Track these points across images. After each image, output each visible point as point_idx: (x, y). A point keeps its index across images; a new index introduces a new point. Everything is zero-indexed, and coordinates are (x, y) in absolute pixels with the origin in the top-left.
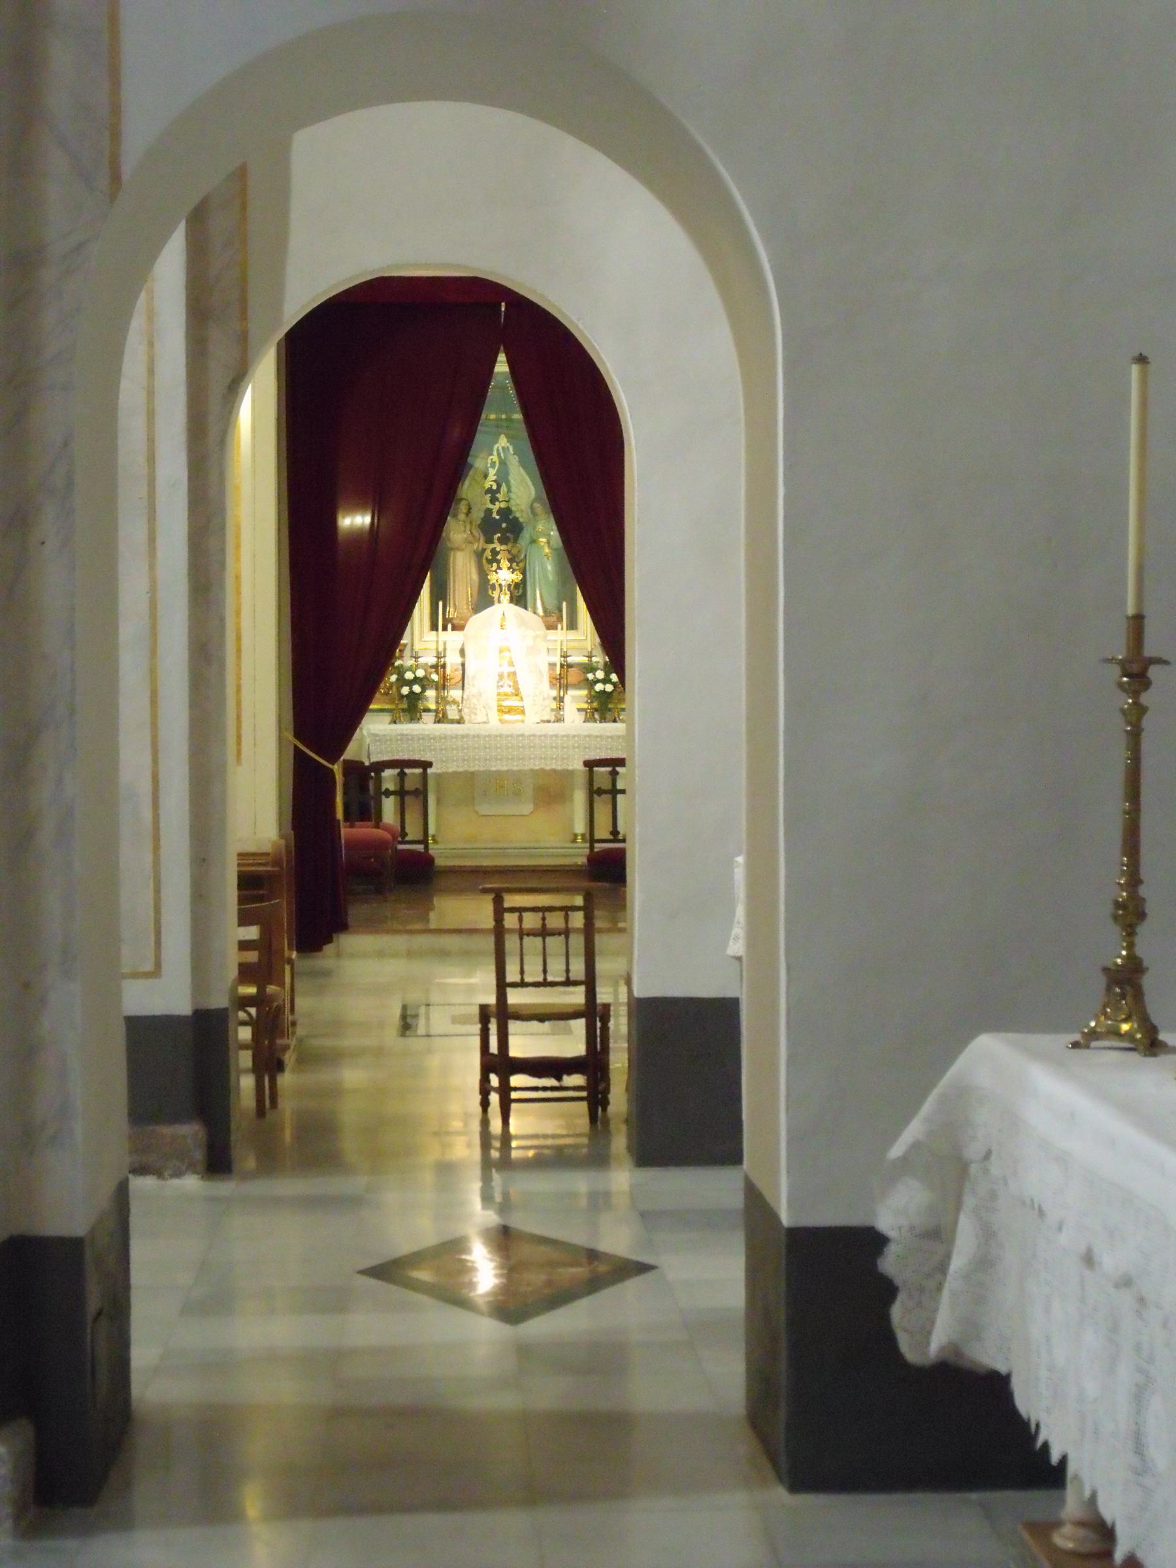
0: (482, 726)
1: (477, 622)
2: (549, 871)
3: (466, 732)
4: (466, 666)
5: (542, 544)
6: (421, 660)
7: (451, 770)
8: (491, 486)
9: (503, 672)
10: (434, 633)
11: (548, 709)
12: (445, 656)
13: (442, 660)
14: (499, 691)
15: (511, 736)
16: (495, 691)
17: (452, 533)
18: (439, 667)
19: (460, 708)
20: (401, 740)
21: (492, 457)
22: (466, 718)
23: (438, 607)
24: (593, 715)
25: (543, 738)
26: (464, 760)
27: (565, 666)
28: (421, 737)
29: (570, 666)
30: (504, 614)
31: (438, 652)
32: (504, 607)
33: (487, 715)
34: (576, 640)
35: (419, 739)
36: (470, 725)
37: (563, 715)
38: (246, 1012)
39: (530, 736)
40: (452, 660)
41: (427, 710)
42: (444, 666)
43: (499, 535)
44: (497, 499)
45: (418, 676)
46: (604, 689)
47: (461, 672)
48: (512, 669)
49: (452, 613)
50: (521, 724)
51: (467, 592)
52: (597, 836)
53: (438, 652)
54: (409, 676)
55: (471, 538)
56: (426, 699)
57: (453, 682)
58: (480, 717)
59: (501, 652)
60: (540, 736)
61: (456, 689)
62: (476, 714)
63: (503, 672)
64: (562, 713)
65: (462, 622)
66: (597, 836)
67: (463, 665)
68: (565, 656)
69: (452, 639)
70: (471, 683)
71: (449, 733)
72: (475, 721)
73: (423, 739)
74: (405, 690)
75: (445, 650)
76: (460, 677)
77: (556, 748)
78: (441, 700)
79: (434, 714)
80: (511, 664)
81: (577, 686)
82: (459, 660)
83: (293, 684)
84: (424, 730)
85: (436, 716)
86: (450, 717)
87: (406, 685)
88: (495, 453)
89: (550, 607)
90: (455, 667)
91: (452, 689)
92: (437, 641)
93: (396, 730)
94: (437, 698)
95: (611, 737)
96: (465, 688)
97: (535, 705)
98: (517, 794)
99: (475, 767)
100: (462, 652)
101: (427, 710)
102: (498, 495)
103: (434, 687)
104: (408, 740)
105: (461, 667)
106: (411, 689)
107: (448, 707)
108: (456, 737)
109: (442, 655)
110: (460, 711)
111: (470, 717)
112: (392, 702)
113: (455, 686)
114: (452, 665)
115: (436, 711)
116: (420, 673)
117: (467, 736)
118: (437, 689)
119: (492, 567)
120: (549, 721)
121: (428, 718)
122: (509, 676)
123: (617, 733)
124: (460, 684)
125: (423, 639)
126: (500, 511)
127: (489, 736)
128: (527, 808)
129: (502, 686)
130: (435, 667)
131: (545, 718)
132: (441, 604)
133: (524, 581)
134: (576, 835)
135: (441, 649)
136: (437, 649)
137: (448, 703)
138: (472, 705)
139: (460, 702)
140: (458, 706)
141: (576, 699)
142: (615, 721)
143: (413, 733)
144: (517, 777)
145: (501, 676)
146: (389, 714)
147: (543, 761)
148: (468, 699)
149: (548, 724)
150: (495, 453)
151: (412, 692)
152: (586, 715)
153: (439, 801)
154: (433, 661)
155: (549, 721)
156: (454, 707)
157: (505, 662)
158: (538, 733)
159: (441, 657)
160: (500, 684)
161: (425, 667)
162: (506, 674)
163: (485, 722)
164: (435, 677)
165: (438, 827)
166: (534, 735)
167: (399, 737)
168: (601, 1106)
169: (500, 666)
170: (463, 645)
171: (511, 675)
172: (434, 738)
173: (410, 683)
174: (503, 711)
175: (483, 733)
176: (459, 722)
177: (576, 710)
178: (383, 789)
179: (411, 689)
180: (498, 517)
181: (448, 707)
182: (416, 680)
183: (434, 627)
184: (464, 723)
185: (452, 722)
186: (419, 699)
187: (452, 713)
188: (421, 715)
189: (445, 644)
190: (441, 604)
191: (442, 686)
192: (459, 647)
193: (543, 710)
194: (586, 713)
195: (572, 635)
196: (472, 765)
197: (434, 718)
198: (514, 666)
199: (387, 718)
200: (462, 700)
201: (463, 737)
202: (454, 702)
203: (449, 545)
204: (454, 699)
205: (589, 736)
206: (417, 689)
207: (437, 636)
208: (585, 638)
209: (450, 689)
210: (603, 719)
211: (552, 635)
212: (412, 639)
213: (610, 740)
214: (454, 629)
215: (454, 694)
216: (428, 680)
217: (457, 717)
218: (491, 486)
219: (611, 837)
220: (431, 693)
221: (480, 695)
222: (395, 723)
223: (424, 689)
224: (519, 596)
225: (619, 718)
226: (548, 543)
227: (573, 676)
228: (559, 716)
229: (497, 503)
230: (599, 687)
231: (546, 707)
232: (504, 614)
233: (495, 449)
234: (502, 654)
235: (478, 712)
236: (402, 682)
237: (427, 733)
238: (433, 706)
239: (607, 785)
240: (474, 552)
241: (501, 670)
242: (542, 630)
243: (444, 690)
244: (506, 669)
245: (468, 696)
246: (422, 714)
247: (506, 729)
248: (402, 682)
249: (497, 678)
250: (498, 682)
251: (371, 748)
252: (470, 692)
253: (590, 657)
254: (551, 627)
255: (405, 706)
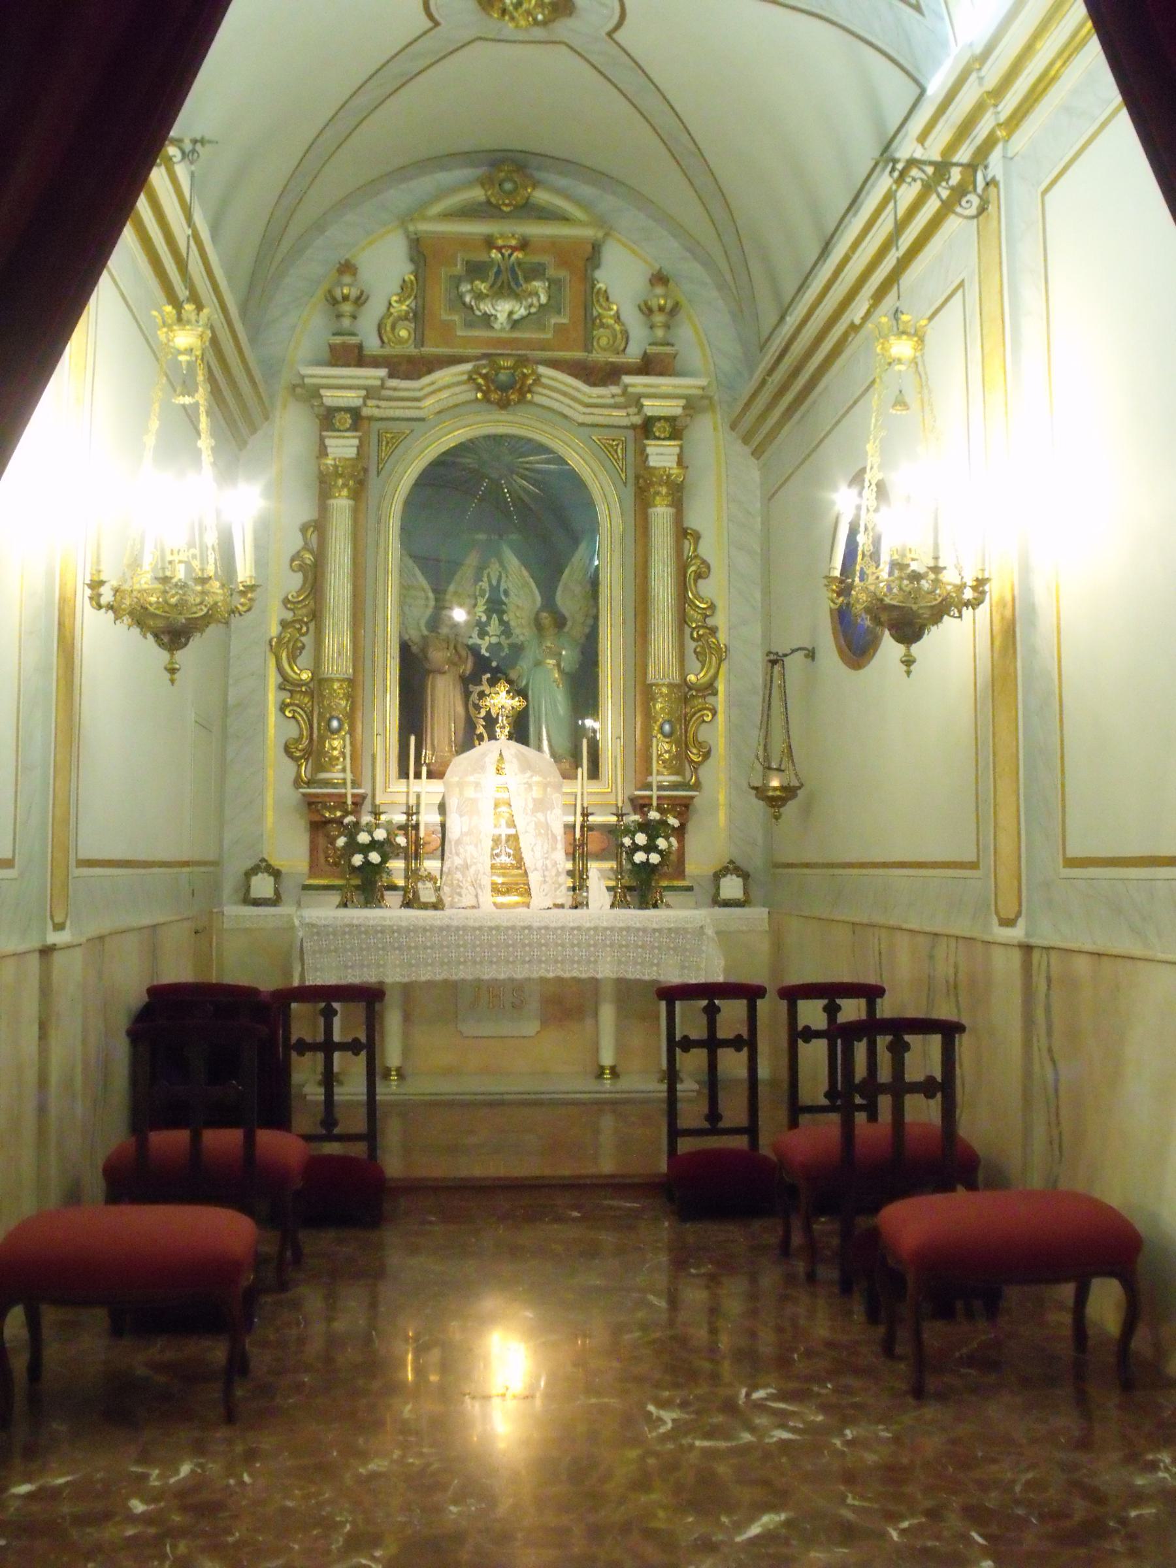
0: (469, 911)
1: (461, 764)
2: (597, 1186)
3: (446, 922)
4: (447, 825)
5: (550, 667)
6: (383, 818)
7: (423, 979)
8: (480, 617)
9: (500, 835)
10: (404, 781)
11: (563, 889)
12: (418, 813)
13: (414, 817)
14: (494, 862)
15: (513, 928)
16: (488, 862)
17: (431, 649)
18: (410, 828)
19: (438, 885)
20: (350, 933)
21: (481, 583)
22: (447, 900)
23: (408, 745)
24: (625, 897)
25: (559, 932)
26: (442, 964)
27: (586, 828)
28: (379, 928)
29: (591, 828)
30: (501, 754)
31: (408, 807)
32: (503, 745)
33: (477, 896)
34: (598, 793)
35: (377, 932)
36: (454, 911)
37: (587, 897)
38: (923, 171)
39: (540, 928)
40: (428, 818)
41: (393, 888)
42: (416, 827)
43: (488, 675)
44: (487, 634)
45: (376, 838)
46: (648, 859)
47: (440, 835)
48: (512, 831)
49: (427, 754)
50: (525, 910)
51: (450, 729)
52: (683, 1123)
53: (408, 807)
54: (363, 838)
55: (456, 659)
56: (389, 873)
57: (429, 848)
58: (468, 900)
59: (496, 806)
60: (556, 929)
61: (434, 859)
62: (460, 895)
63: (500, 835)
64: (585, 894)
65: (441, 768)
66: (683, 1123)
67: (443, 826)
68: (585, 814)
69: (428, 790)
70: (454, 851)
71: (421, 923)
72: (460, 905)
73: (382, 932)
74: (358, 860)
75: (418, 805)
76: (439, 842)
77: (578, 945)
78: (412, 874)
79: (402, 893)
80: (512, 824)
81: (600, 856)
82: (437, 818)
83: (1161, 857)
84: (384, 918)
85: (405, 896)
86: (423, 899)
87: (360, 852)
88: (485, 579)
89: (560, 751)
90: (432, 829)
91: (429, 859)
92: (408, 793)
93: (343, 918)
94: (407, 870)
95: (659, 930)
96: (446, 857)
97: (545, 882)
98: (518, 1006)
99: (463, 973)
100: (442, 808)
101: (393, 888)
102: (488, 629)
103: (402, 855)
104: (361, 933)
105: (439, 829)
106: (366, 857)
107: (420, 885)
108: (431, 929)
109: (414, 811)
110: (438, 889)
111: (453, 898)
112: (342, 877)
113: (431, 855)
114: (426, 825)
115: (405, 889)
116: (380, 835)
117: (448, 928)
118: (406, 858)
119: (479, 713)
120: (562, 906)
121: (393, 899)
122: (507, 841)
123: (667, 925)
124: (439, 852)
125: (389, 790)
126: (490, 647)
127: (480, 928)
128: (531, 1027)
129: (497, 855)
130: (403, 828)
131: (559, 901)
132: (413, 739)
133: (527, 706)
134: (602, 1068)
135: (412, 801)
136: (407, 804)
137: (420, 878)
138: (455, 882)
139: (438, 877)
140: (435, 883)
141: (599, 875)
142: (655, 906)
143: (367, 923)
144: (517, 988)
145: (496, 841)
146: (339, 892)
147: (559, 965)
148: (449, 873)
149: (561, 911)
150: (485, 579)
151: (367, 863)
152: (615, 896)
153: (407, 1018)
154: (402, 819)
155: (562, 906)
156: (429, 885)
157: (503, 822)
158: (553, 925)
159: (412, 814)
160: (495, 852)
161: (389, 826)
162: (503, 838)
163: (473, 907)
164: (401, 840)
165: (406, 1051)
166: (547, 928)
167: (347, 930)
168: (416, 736)
169: (495, 826)
170: (443, 798)
171: (512, 839)
172: (399, 931)
173: (365, 849)
174: (499, 891)
175: (471, 923)
176: (437, 906)
177: (605, 890)
178: (294, 1039)
179: (366, 857)
180: (487, 654)
181: (420, 885)
182: (374, 845)
183: (404, 774)
184: (443, 909)
185: (425, 906)
186: (377, 873)
187: (426, 893)
188: (382, 896)
189: (418, 796)
190: (413, 739)
191: (414, 852)
192: (438, 800)
193: (556, 889)
194: (616, 893)
195: (593, 787)
196: (454, 971)
197: (401, 899)
198: (515, 826)
199: (336, 898)
200: (441, 875)
201: (441, 929)
202: (430, 878)
203: (427, 666)
204: (430, 873)
205: (628, 929)
206: (375, 857)
207: (408, 785)
208: (609, 790)
209: (424, 859)
210: (643, 904)
211: (568, 787)
212: (374, 790)
213: (657, 934)
214: (430, 775)
215: (431, 865)
216: (391, 844)
217: (433, 900)
218: (480, 617)
219: (706, 1125)
220: (397, 865)
221: (466, 867)
222: (345, 906)
223: (385, 859)
224: (521, 731)
225: (662, 902)
226: (558, 665)
227: (595, 842)
228: (579, 899)
229: (487, 638)
230: (639, 857)
231: (560, 885)
232: (501, 754)
233: (485, 575)
234: (499, 810)
235: (464, 892)
236: (353, 847)
237: (388, 923)
238: (401, 882)
239: (698, 1032)
240: (460, 677)
241: (497, 832)
242: (554, 775)
243: (416, 859)
244: (505, 831)
245: (449, 868)
246: (385, 893)
247: (505, 918)
248: (353, 847)
249: (491, 843)
250: (492, 849)
251: (305, 944)
252: (453, 863)
253: (620, 815)
254: (569, 775)
255: (357, 882)
